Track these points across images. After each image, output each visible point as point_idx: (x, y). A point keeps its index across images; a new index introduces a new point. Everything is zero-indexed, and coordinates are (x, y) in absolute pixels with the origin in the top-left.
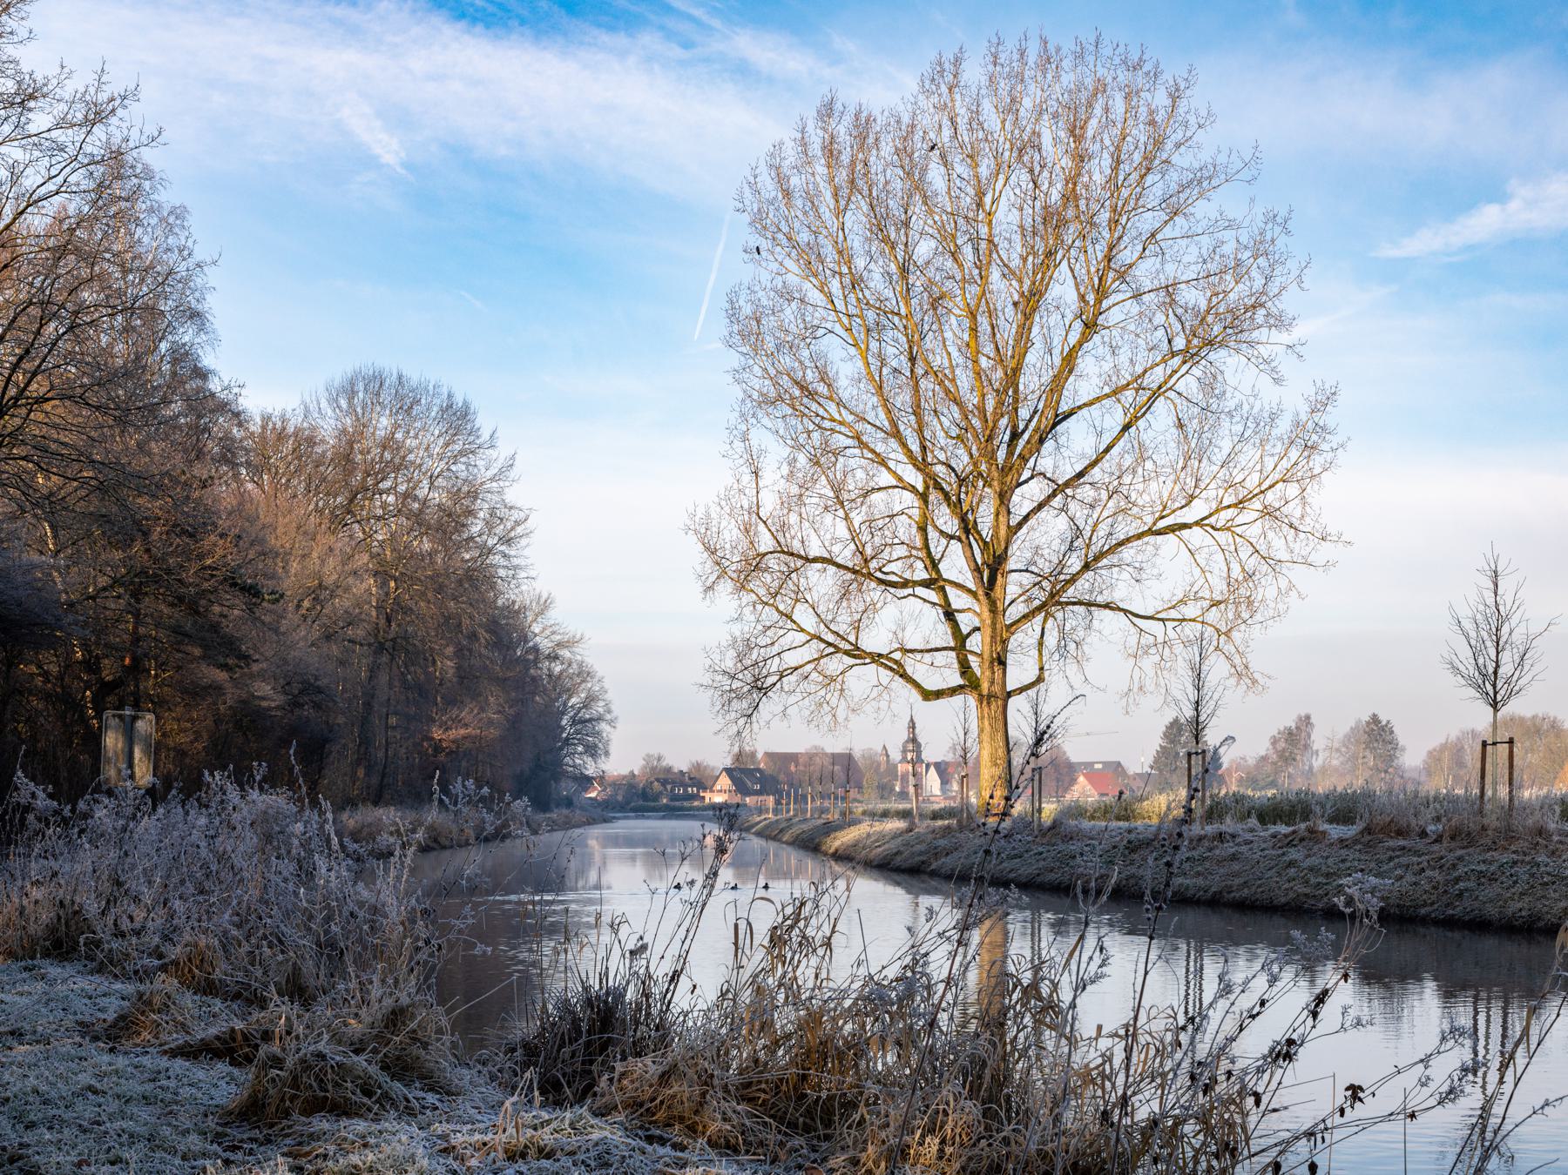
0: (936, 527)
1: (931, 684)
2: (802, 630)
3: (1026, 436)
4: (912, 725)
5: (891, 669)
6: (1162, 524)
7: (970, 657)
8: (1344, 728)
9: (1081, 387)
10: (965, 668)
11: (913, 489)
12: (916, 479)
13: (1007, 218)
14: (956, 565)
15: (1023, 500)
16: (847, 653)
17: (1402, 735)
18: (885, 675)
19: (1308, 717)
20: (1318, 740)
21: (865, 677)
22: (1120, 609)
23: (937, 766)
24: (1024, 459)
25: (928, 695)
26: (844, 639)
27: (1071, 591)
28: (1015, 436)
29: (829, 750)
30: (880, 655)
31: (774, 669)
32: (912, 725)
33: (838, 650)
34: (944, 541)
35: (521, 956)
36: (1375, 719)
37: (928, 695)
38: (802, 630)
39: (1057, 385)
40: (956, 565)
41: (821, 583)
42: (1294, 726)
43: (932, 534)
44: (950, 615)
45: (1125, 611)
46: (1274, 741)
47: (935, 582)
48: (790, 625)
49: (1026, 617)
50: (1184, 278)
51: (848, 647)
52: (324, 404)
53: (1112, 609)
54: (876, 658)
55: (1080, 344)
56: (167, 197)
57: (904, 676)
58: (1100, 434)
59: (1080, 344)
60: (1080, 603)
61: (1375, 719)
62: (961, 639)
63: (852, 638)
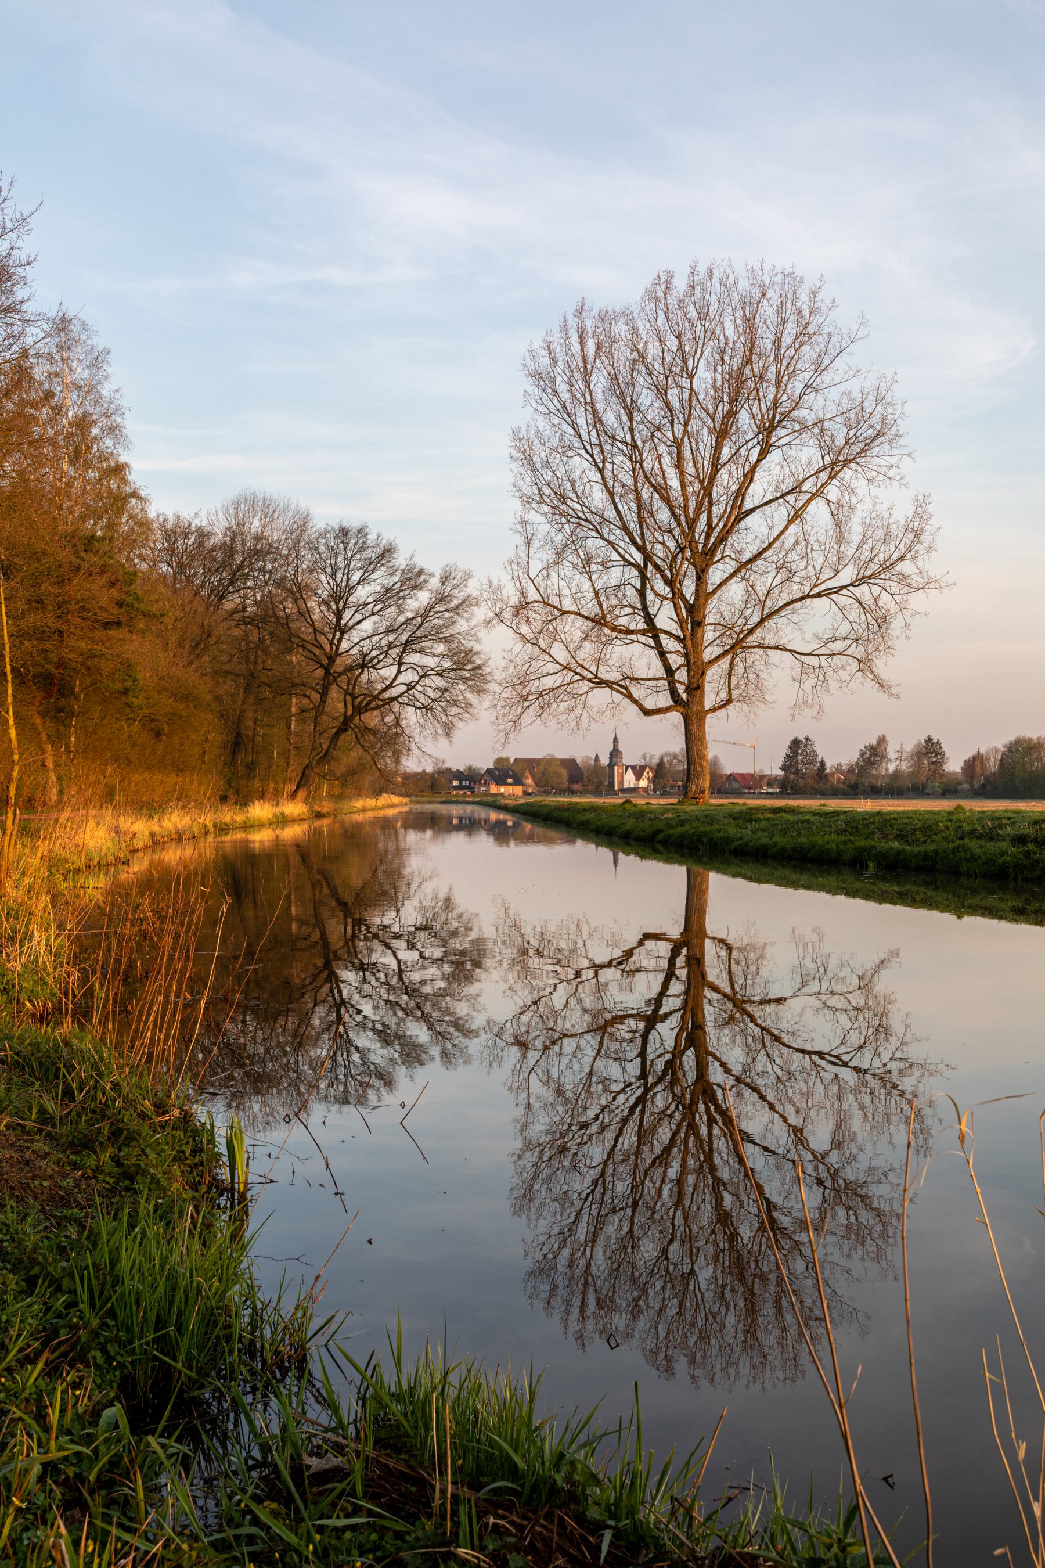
0: (652, 589)
1: (649, 704)
2: (557, 662)
3: (718, 530)
4: (616, 740)
5: (622, 693)
6: (816, 590)
7: (678, 685)
8: (909, 747)
9: (756, 494)
10: (674, 693)
11: (636, 566)
12: (638, 557)
13: (704, 378)
14: (666, 618)
15: (716, 574)
16: (590, 680)
17: (946, 748)
18: (618, 697)
19: (884, 737)
20: (891, 752)
21: (603, 695)
22: (786, 650)
23: (633, 768)
24: (715, 546)
25: (647, 712)
26: (587, 670)
27: (750, 639)
28: (710, 527)
29: (558, 757)
30: (613, 683)
31: (533, 690)
32: (616, 740)
33: (584, 678)
34: (658, 601)
35: (277, 1431)
36: (929, 740)
37: (647, 712)
38: (557, 662)
39: (740, 494)
40: (666, 618)
41: (574, 628)
42: (875, 743)
43: (650, 596)
44: (662, 655)
45: (791, 651)
46: (862, 754)
47: (652, 630)
48: (547, 658)
49: (718, 658)
50: (828, 416)
51: (590, 676)
52: (221, 515)
53: (781, 649)
54: (608, 684)
55: (758, 461)
56: (99, 342)
57: (629, 696)
58: (771, 528)
59: (758, 461)
60: (758, 647)
61: (929, 740)
62: (670, 671)
63: (593, 669)
